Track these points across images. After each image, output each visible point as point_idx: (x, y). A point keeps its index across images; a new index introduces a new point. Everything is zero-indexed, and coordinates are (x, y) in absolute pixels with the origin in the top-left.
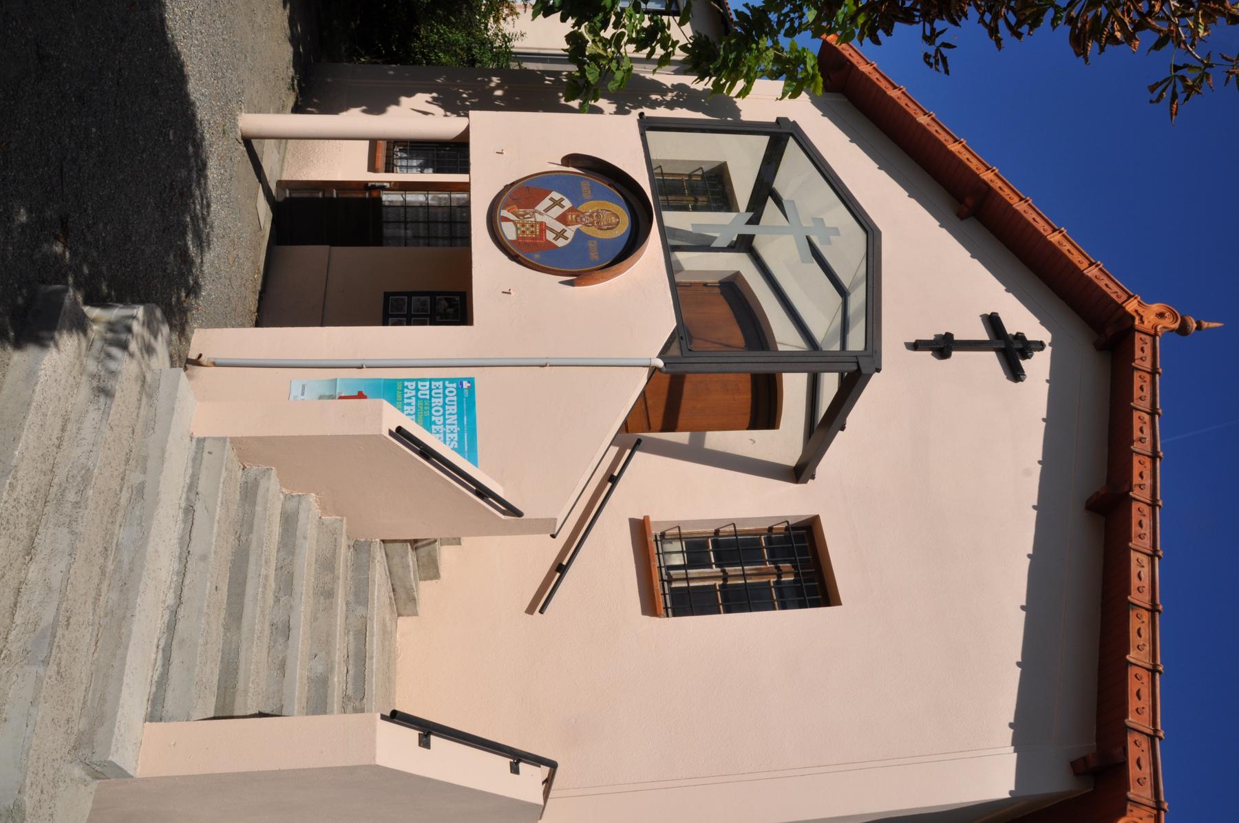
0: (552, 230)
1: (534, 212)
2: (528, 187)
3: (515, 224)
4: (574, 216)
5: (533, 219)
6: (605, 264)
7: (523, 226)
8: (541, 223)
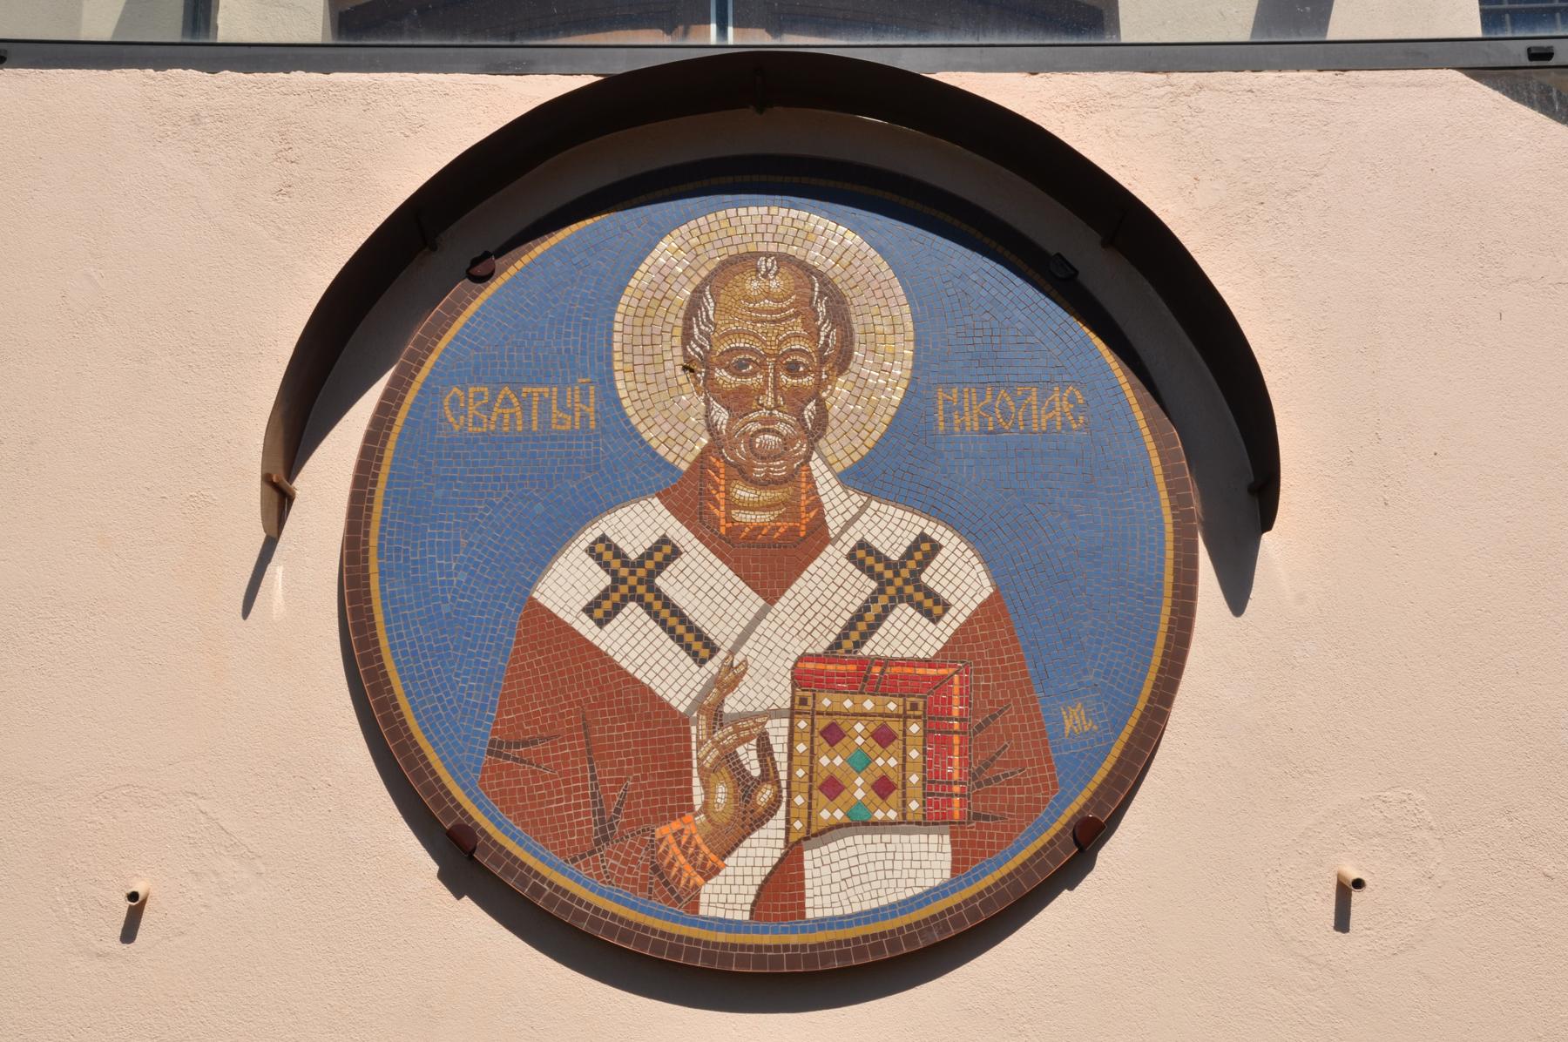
0: (864, 623)
1: (716, 717)
2: (495, 749)
3: (821, 834)
4: (743, 493)
5: (778, 731)
6: (1109, 357)
7: (833, 787)
8: (807, 676)
